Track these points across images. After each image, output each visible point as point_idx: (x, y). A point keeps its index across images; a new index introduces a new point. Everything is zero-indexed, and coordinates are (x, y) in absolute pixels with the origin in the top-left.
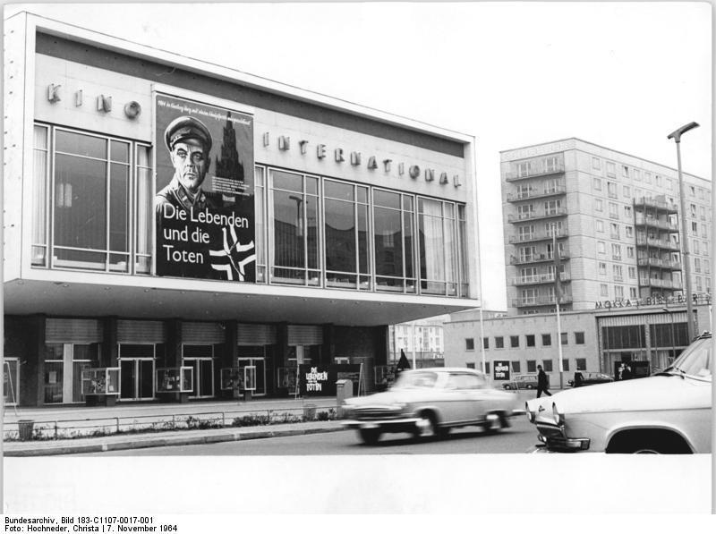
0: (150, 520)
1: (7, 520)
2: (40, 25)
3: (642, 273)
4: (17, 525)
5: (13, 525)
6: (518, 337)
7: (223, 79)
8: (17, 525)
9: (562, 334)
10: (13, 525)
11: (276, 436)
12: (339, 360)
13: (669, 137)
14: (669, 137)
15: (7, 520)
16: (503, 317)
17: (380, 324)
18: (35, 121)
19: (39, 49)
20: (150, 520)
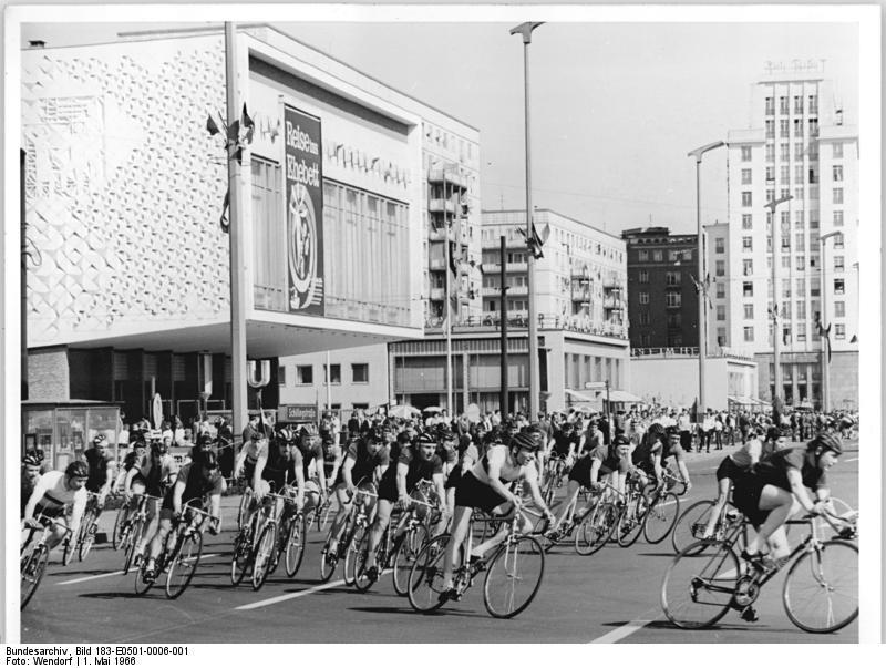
0: (184, 651)
1: (9, 650)
2: (254, 48)
3: (235, 536)
4: (21, 657)
5: (15, 657)
6: (355, 380)
7: (350, 98)
8: (21, 657)
9: (332, 366)
10: (15, 657)
11: (818, 198)
12: (99, 466)
13: (689, 155)
14: (689, 155)
15: (9, 650)
16: (660, 263)
17: (722, 459)
18: (252, 154)
19: (251, 68)
20: (184, 651)
